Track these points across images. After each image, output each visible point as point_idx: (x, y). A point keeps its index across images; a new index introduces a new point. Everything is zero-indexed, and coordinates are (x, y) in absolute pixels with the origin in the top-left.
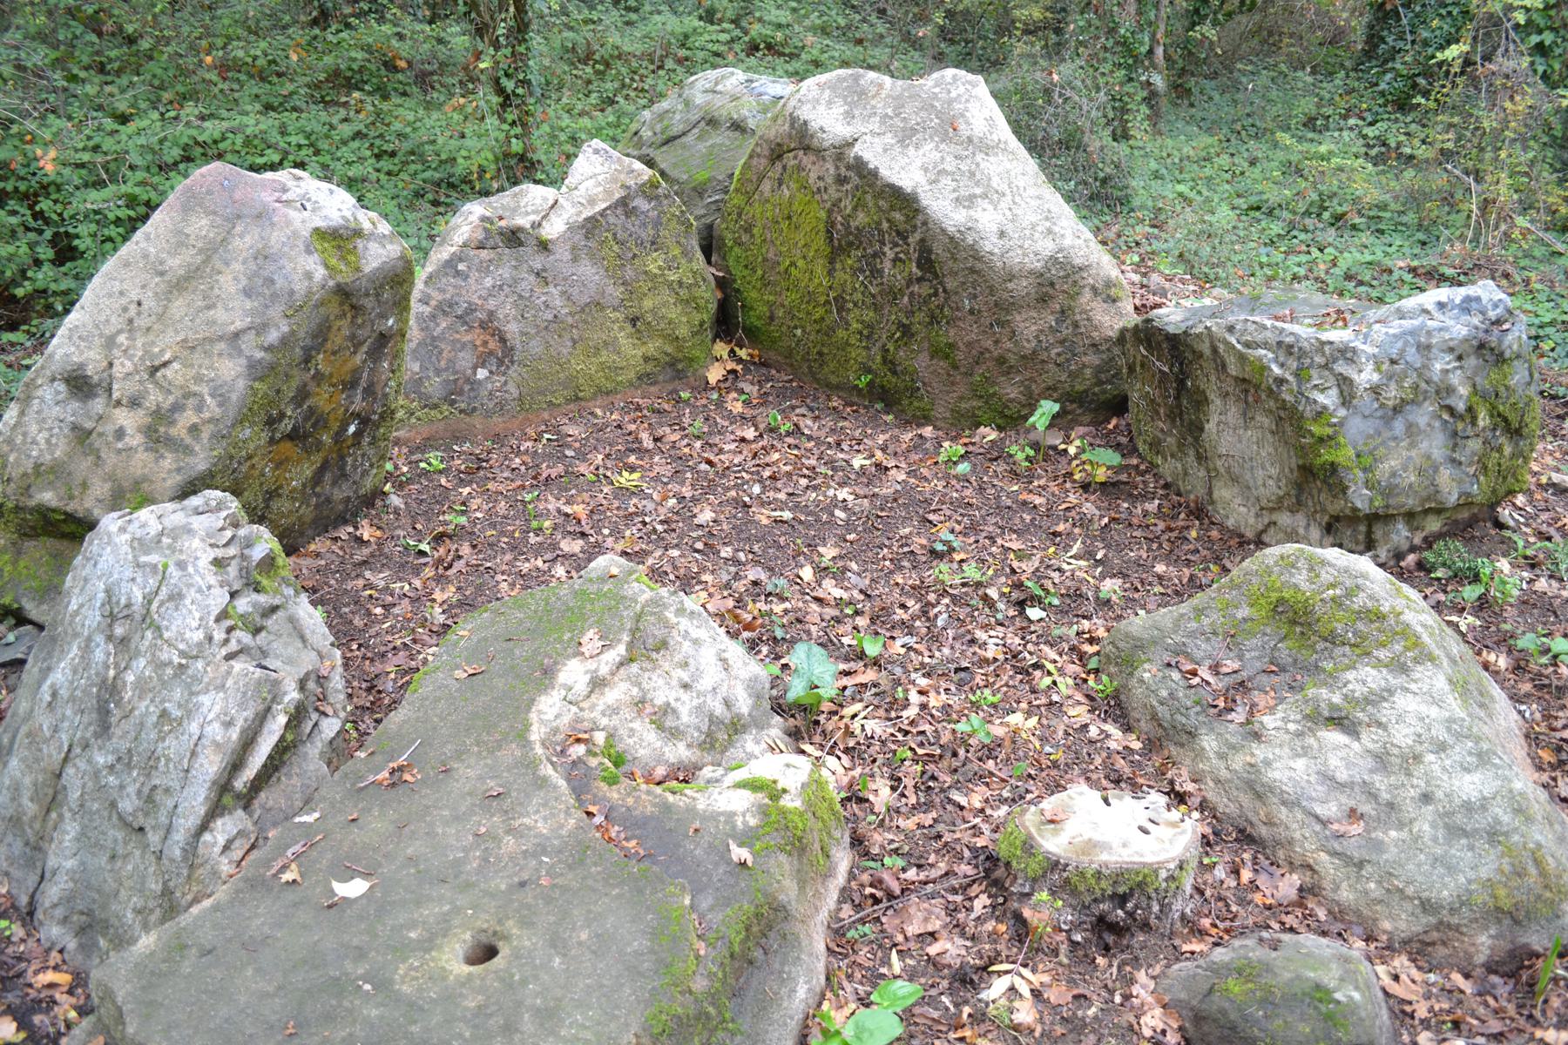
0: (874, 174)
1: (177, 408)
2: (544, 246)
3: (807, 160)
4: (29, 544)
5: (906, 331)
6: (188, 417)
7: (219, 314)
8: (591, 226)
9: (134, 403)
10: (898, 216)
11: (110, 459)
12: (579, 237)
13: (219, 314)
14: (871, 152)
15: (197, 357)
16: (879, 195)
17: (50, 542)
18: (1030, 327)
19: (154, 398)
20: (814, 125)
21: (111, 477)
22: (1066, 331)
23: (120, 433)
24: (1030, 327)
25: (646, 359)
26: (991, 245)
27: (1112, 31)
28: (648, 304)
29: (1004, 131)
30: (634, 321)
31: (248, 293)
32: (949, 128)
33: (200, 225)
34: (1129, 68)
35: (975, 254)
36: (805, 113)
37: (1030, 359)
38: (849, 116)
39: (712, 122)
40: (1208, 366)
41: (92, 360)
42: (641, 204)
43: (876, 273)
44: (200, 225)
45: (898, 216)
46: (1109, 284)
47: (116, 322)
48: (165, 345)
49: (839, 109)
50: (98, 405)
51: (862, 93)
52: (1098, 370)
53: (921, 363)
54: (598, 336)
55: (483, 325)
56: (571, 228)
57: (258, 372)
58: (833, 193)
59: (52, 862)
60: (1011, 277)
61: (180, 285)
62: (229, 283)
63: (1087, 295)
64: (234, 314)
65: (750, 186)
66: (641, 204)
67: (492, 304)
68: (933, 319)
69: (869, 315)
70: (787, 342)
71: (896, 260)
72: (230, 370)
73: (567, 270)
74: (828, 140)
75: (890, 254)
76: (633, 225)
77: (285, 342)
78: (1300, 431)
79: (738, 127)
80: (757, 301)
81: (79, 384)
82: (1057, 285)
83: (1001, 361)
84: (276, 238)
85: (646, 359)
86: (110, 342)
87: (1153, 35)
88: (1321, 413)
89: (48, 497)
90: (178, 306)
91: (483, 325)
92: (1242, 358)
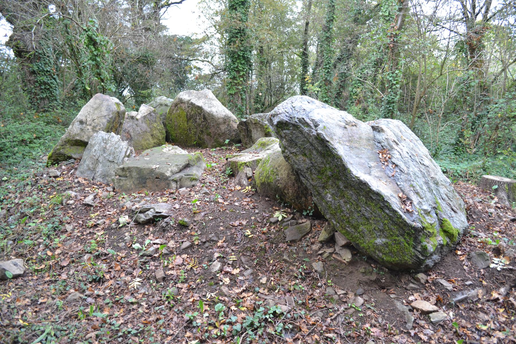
0: (194, 104)
1: (97, 126)
2: (137, 120)
3: (182, 105)
4: (72, 147)
5: (202, 131)
6: (98, 127)
7: (102, 113)
8: (145, 117)
9: (90, 125)
10: (199, 111)
11: (87, 133)
12: (143, 119)
13: (102, 113)
14: (194, 101)
15: (99, 119)
16: (196, 108)
17: (76, 147)
18: (223, 128)
19: (93, 124)
20: (183, 98)
21: (87, 135)
22: (229, 128)
23: (88, 129)
24: (223, 128)
25: (154, 143)
26: (215, 114)
27: (236, 106)
28: (154, 132)
29: (215, 97)
30: (152, 135)
31: (106, 110)
32: (206, 97)
33: (98, 101)
34: (241, 114)
35: (213, 116)
36: (181, 97)
37: (223, 133)
38: (189, 96)
39: (161, 105)
40: (250, 124)
41: (84, 119)
42: (152, 114)
43: (196, 122)
44: (98, 101)
45: (199, 111)
46: (235, 120)
47: (87, 114)
48: (95, 117)
49: (187, 95)
50: (84, 125)
51: (191, 93)
52: (235, 135)
53: (205, 137)
54: (146, 138)
55: (128, 133)
56: (141, 117)
57: (109, 122)
58: (187, 109)
59: (97, 170)
60: (219, 119)
61: (96, 109)
62: (103, 109)
63: (232, 122)
64: (105, 113)
65: (171, 113)
66: (152, 114)
67: (129, 129)
68: (207, 128)
69: (195, 130)
70: (180, 140)
71: (199, 119)
72: (104, 121)
73: (141, 124)
74: (186, 100)
75: (198, 118)
76: (151, 118)
77: (112, 117)
78: (264, 128)
79: (166, 105)
80: (173, 133)
81: (81, 122)
82: (226, 120)
83: (219, 134)
84: (110, 103)
85: (154, 143)
86: (86, 116)
87: (246, 107)
88: (266, 125)
89: (78, 138)
90: (96, 112)
91: (128, 133)
92: (254, 120)
